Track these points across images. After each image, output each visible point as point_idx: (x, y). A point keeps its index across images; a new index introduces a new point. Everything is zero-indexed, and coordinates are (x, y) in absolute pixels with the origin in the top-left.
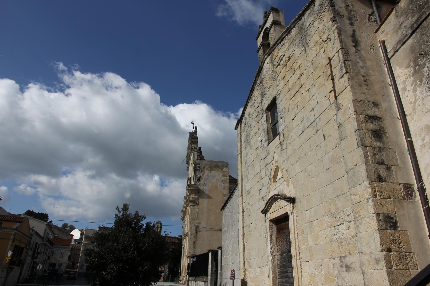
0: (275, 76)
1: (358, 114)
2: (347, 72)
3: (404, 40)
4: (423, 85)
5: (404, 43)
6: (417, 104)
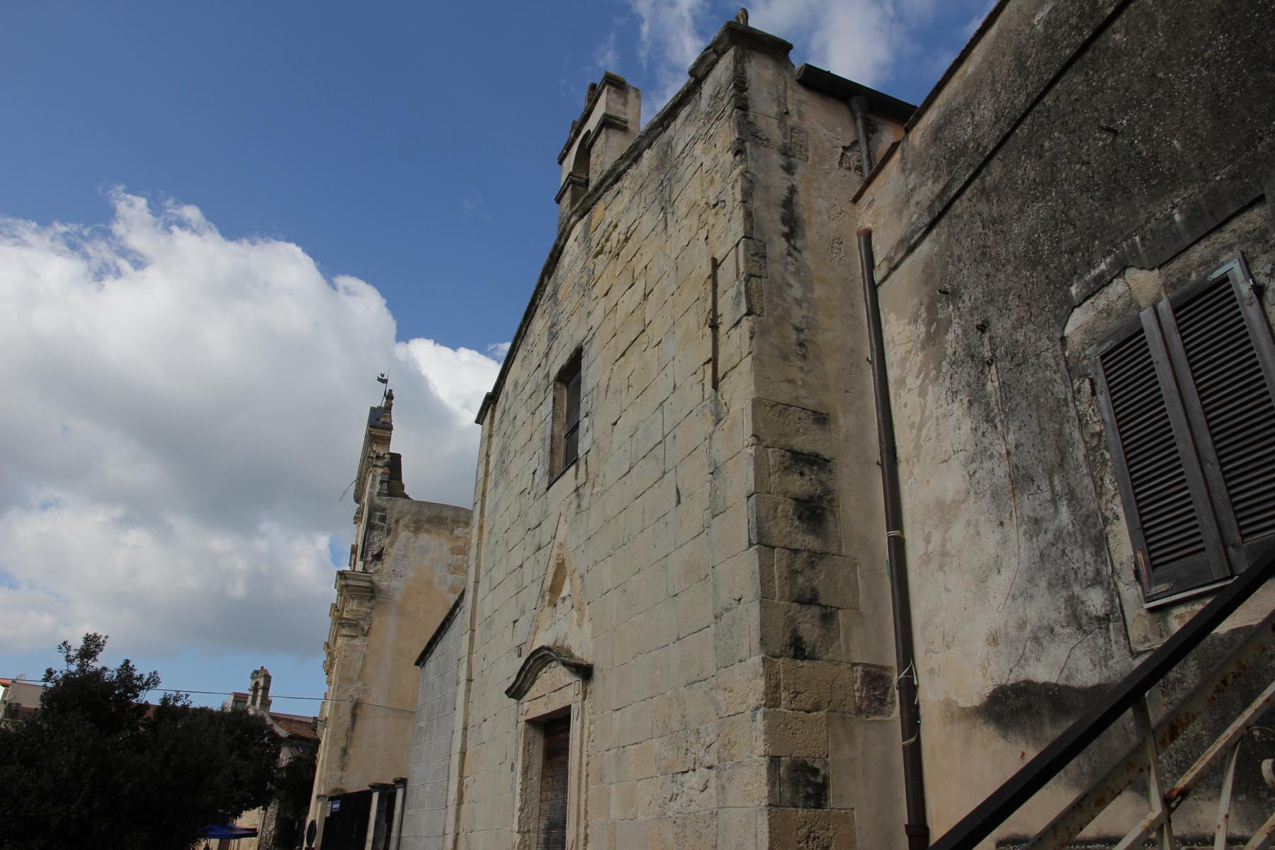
0: (586, 288)
1: (764, 444)
2: (748, 314)
3: (912, 241)
5: (911, 250)
6: (924, 430)
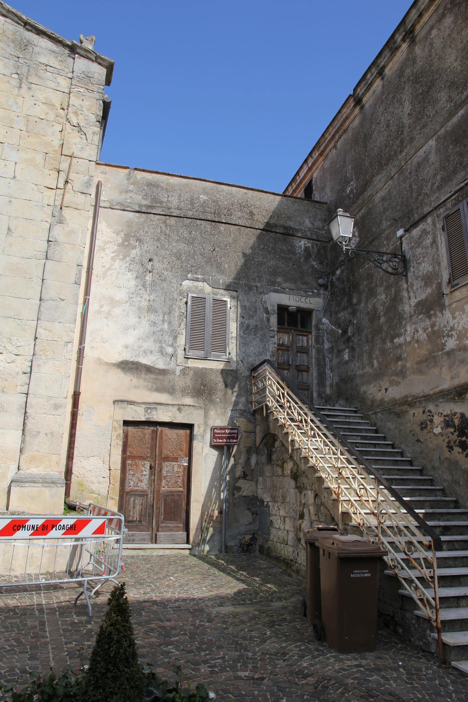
3: (126, 209)
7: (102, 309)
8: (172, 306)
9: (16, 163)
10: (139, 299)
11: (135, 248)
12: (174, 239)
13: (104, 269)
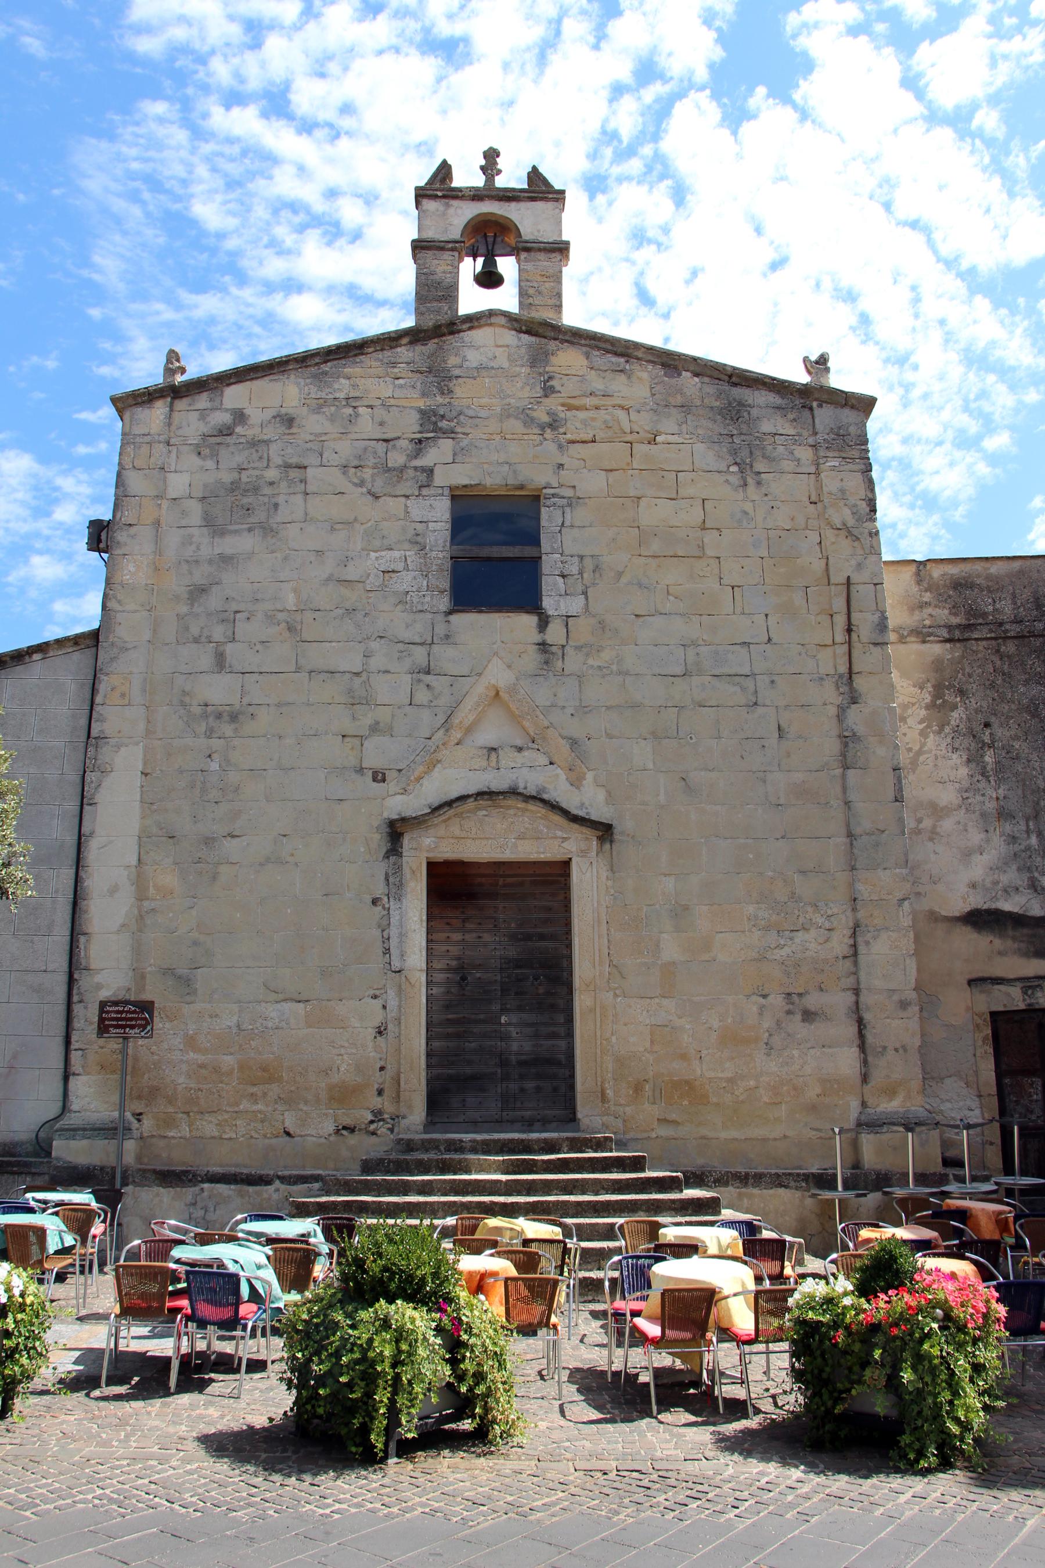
4: (942, 735)
7: (921, 826)
8: (1038, 803)
9: (767, 615)
10: (979, 798)
11: (954, 707)
12: (1019, 681)
13: (911, 755)
